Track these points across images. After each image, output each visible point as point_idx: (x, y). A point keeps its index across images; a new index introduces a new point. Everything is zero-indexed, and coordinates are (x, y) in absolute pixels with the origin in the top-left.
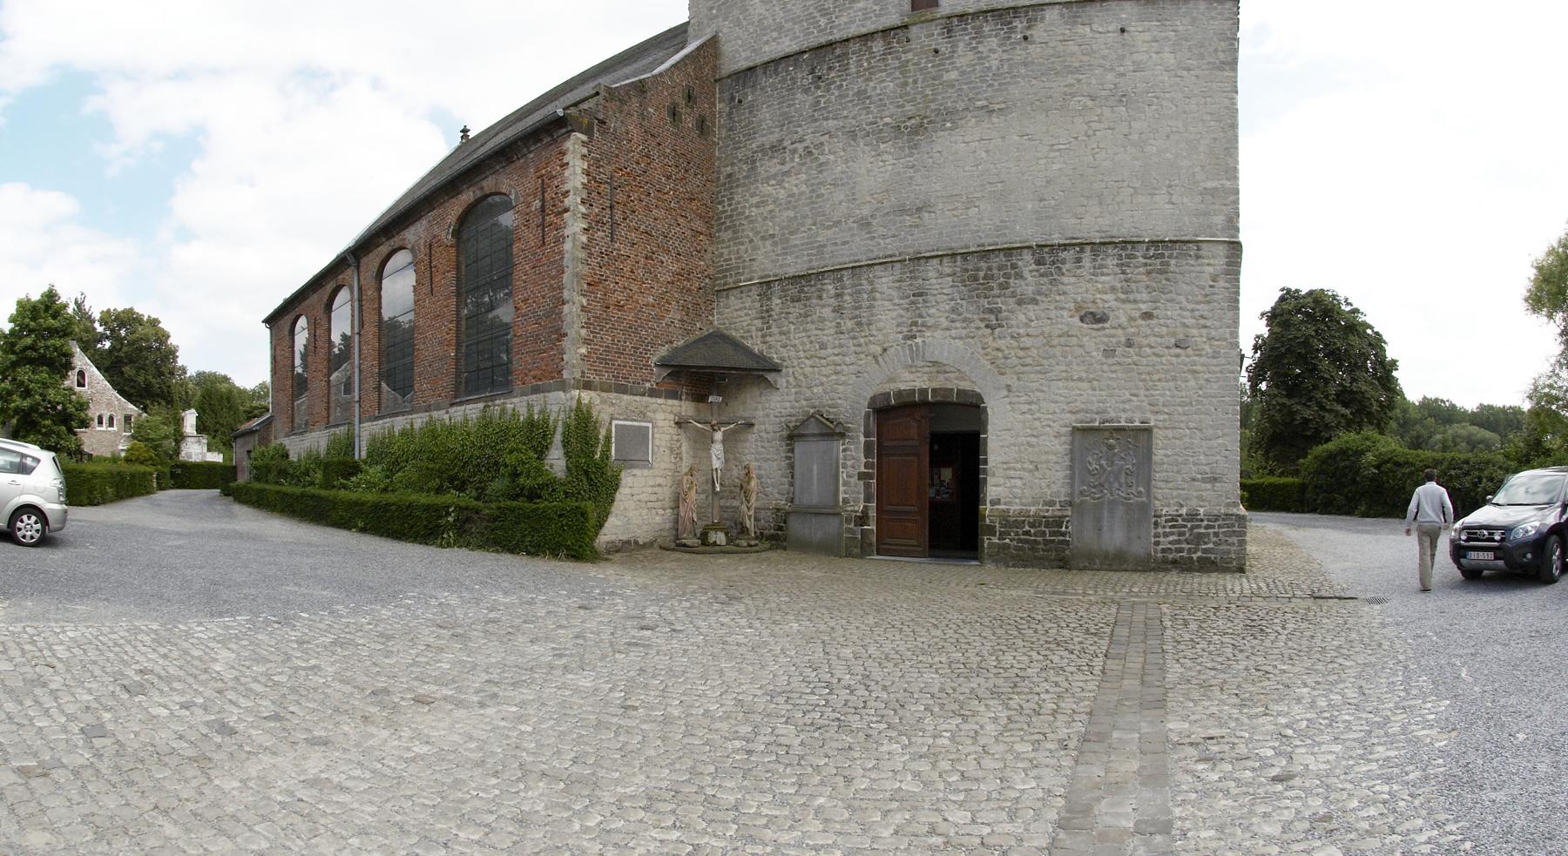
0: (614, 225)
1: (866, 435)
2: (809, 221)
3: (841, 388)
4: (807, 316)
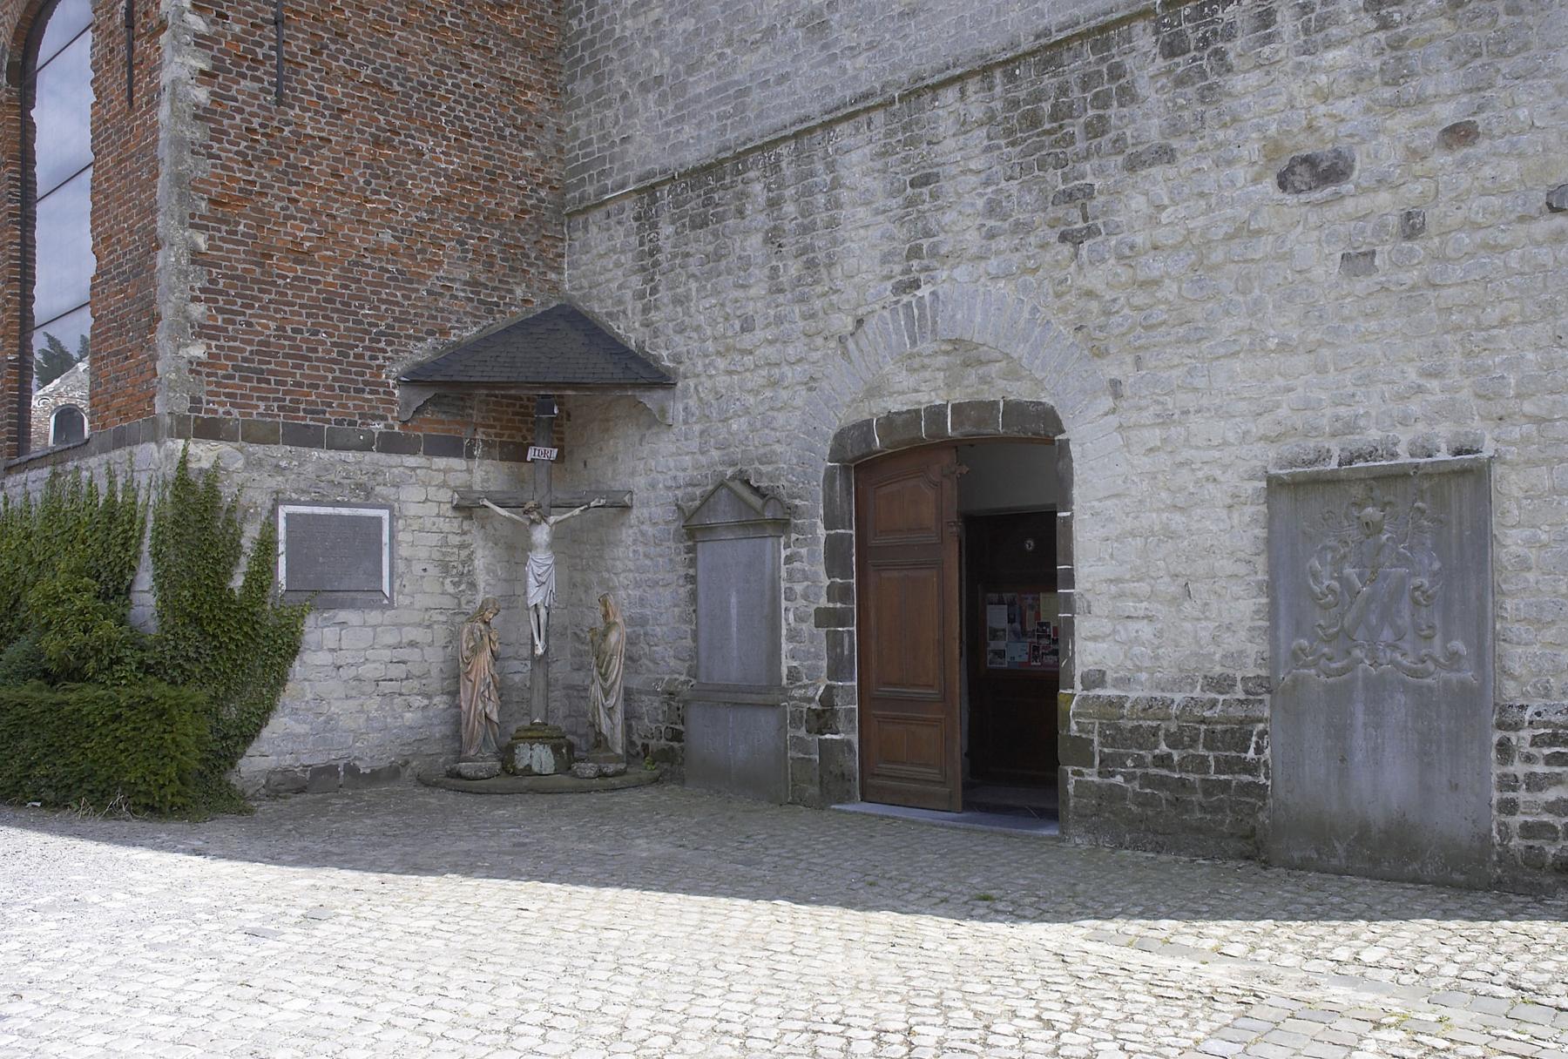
0: (285, 69)
2: (720, 37)
3: (781, 418)
4: (718, 257)
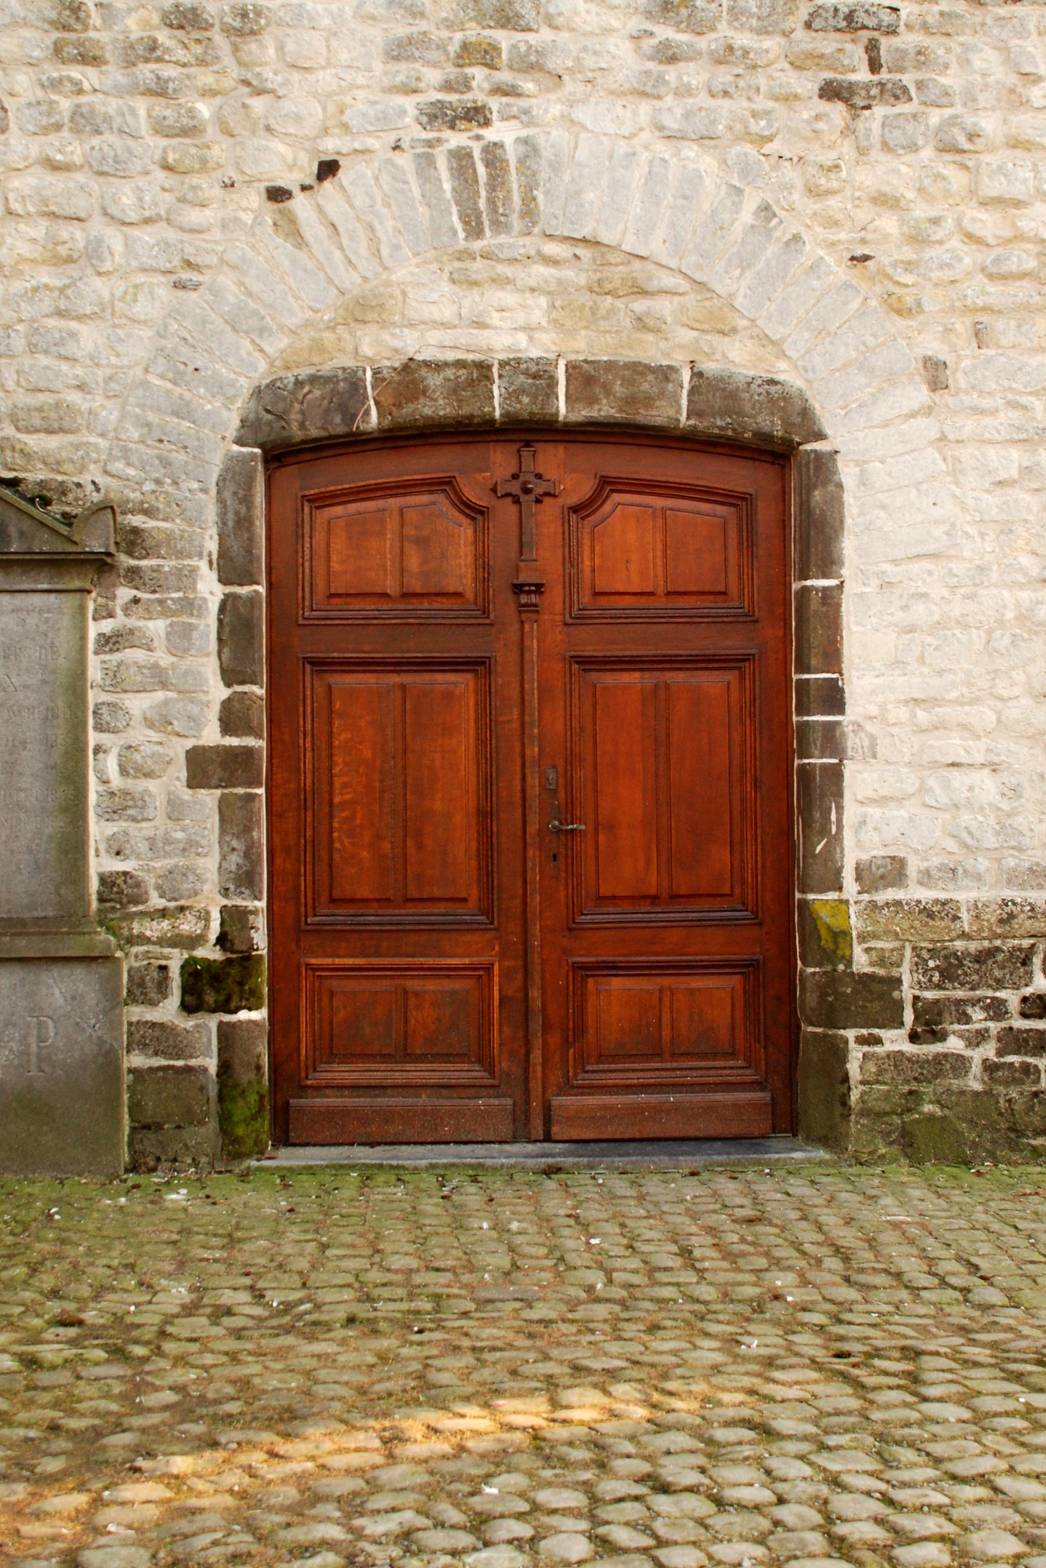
1: (230, 570)
